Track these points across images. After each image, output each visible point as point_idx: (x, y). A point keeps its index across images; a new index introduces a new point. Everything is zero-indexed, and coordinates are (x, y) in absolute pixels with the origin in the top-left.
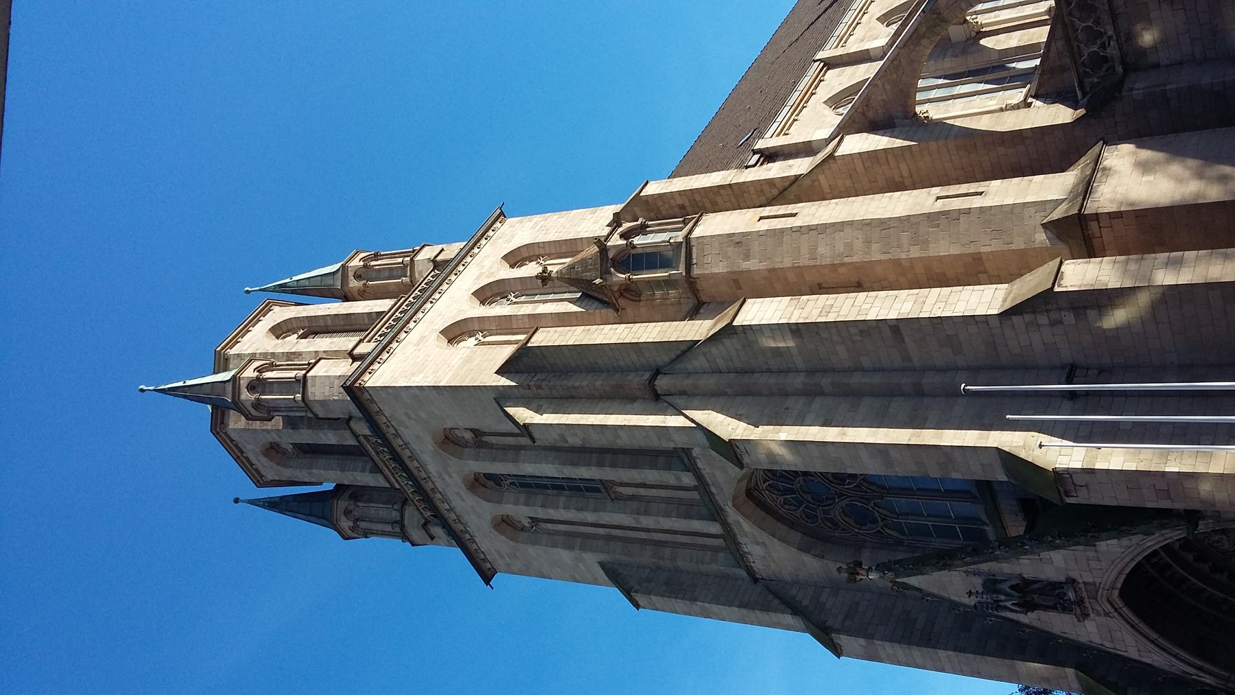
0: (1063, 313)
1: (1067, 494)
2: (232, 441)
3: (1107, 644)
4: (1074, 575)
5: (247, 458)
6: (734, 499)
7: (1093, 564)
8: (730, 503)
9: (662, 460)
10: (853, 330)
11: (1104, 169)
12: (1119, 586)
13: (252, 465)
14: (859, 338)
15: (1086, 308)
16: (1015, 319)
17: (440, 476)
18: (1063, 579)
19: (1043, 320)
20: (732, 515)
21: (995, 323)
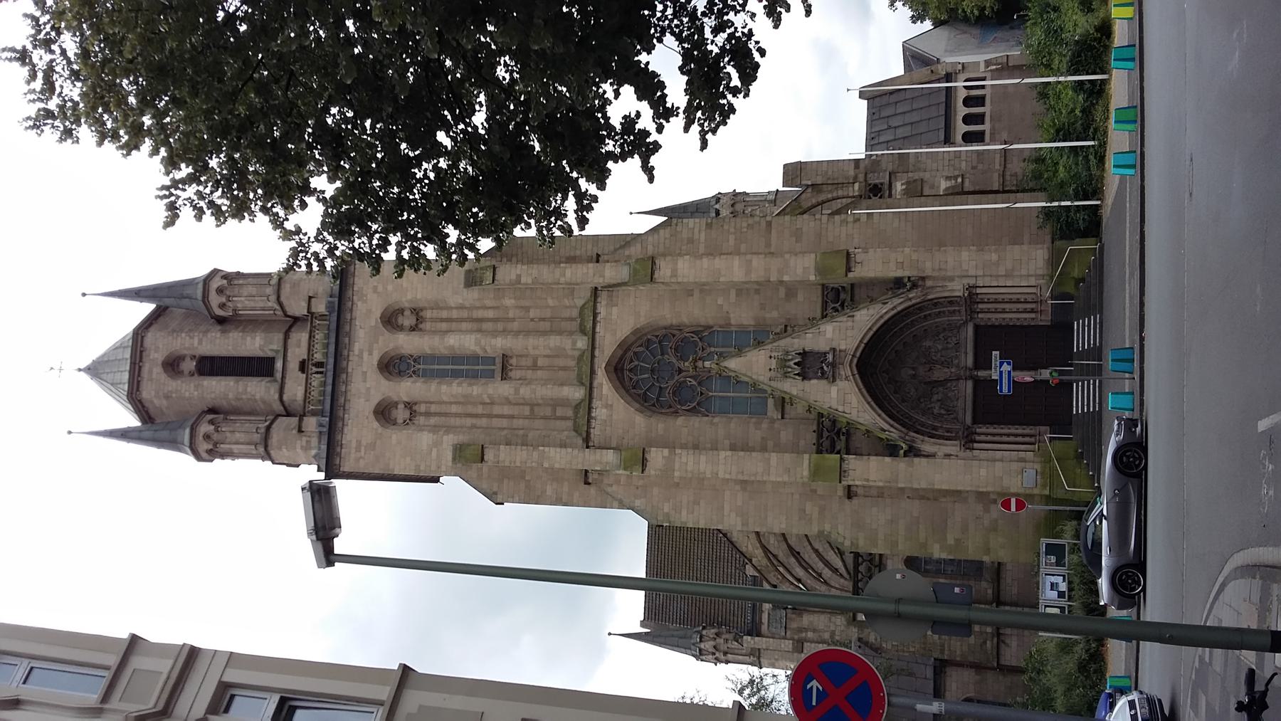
7: (849, 333)
12: (858, 354)
17: (361, 351)
20: (602, 378)
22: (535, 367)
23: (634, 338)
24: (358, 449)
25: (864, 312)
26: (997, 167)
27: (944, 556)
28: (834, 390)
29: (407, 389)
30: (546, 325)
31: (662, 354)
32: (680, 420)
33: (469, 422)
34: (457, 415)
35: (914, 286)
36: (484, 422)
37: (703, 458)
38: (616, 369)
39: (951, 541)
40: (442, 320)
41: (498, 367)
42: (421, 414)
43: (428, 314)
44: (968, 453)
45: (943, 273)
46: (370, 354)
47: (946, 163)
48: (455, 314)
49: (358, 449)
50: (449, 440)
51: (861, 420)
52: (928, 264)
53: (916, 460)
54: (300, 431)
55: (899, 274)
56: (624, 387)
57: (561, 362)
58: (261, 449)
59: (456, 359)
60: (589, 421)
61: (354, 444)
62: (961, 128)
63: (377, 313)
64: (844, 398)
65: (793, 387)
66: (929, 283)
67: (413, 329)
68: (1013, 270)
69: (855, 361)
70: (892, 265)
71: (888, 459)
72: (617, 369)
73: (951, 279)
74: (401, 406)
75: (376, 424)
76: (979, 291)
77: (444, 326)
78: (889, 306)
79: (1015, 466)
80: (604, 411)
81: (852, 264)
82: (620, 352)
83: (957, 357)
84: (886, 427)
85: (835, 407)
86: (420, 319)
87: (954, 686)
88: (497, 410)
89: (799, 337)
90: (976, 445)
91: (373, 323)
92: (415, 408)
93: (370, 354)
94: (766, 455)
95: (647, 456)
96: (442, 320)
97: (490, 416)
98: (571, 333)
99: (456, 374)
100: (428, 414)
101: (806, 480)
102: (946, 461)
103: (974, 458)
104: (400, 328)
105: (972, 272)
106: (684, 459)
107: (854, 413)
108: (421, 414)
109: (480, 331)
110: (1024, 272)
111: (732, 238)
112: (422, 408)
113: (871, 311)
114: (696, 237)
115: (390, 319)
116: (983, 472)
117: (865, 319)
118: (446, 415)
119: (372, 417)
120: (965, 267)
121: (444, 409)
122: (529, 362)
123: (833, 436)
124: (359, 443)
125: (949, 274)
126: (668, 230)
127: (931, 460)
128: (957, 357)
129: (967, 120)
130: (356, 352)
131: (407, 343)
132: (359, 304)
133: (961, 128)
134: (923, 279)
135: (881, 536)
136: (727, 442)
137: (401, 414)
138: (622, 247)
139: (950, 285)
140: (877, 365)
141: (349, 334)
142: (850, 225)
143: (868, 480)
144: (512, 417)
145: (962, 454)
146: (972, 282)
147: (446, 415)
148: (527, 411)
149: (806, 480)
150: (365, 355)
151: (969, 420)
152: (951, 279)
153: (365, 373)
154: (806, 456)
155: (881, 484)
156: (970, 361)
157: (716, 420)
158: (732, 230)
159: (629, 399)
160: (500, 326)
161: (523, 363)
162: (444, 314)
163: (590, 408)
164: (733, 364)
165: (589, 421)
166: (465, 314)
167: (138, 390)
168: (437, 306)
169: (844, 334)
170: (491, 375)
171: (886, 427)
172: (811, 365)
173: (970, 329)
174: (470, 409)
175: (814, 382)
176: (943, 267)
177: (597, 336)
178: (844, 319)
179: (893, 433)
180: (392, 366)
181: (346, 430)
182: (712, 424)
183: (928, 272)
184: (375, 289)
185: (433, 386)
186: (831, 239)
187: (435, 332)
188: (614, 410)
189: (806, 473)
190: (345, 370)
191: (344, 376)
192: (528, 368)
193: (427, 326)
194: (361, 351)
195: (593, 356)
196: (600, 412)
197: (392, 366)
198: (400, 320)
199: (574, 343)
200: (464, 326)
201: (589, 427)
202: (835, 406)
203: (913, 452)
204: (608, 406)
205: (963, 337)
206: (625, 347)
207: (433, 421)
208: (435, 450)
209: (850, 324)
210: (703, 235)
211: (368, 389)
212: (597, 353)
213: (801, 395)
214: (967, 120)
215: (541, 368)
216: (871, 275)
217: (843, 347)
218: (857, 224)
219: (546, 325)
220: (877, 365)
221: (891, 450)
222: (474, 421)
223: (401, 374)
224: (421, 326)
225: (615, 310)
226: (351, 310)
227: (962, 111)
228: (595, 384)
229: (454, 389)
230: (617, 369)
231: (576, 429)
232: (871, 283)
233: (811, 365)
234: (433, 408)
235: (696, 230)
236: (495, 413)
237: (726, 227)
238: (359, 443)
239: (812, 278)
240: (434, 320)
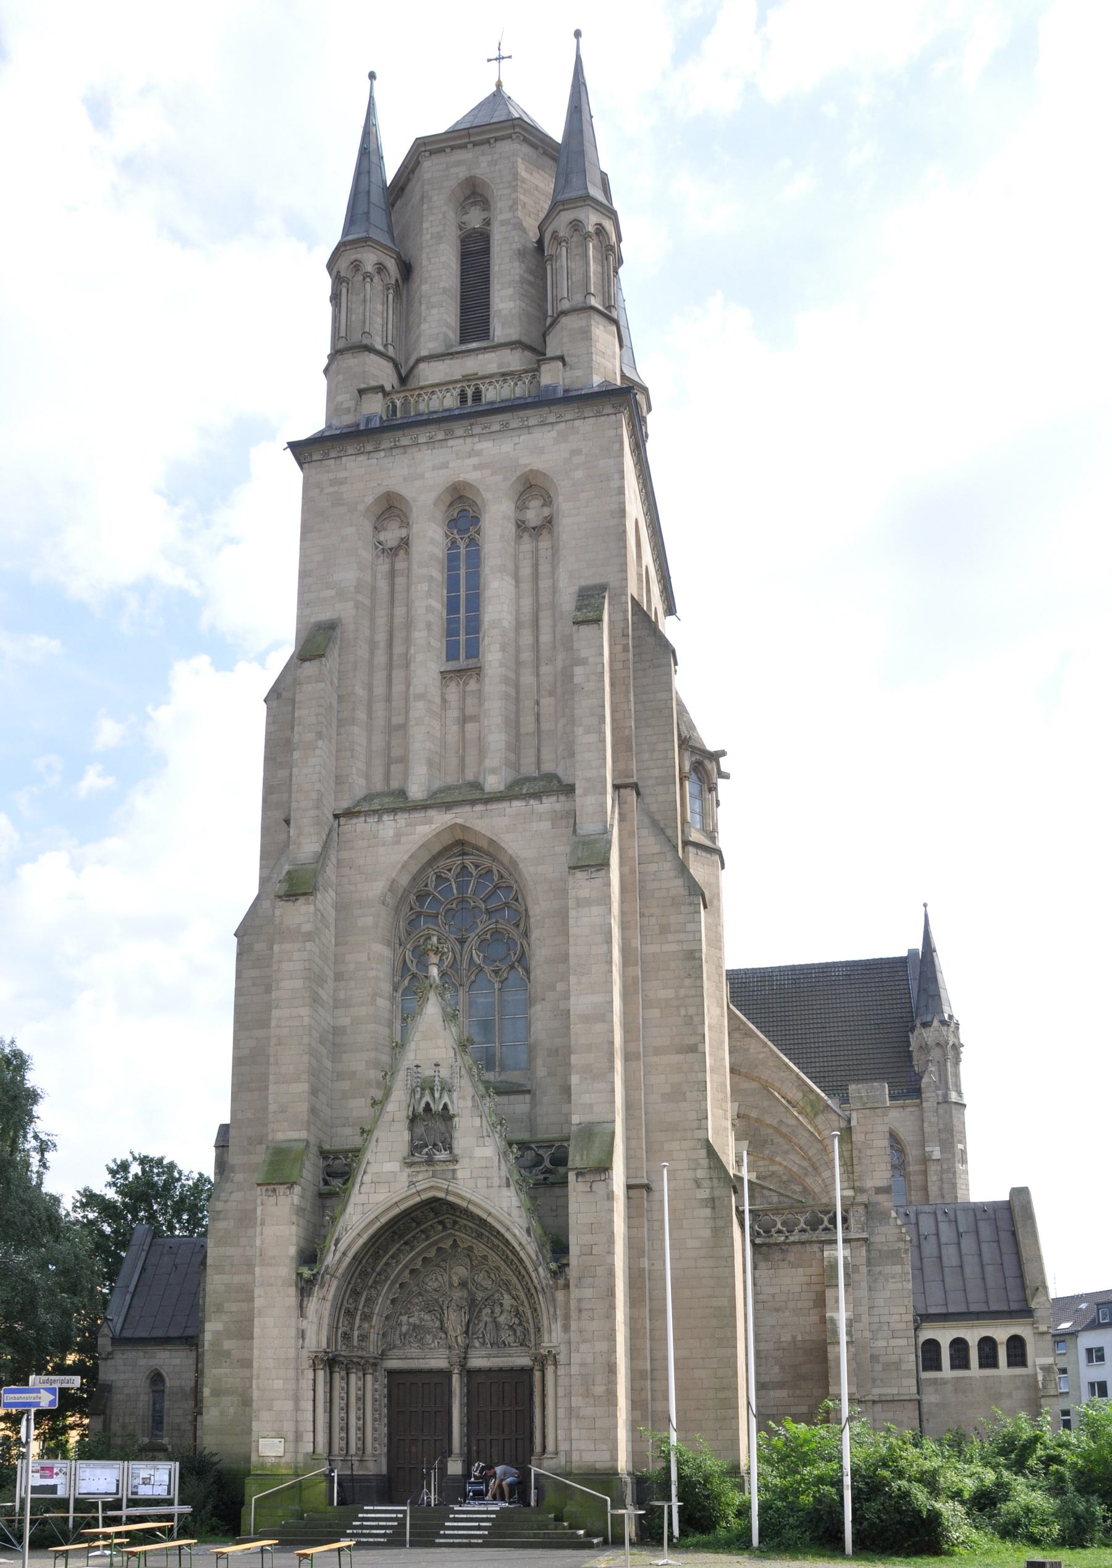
0: (708, 1190)
1: (577, 1175)
2: (497, 139)
3: (367, 1178)
4: (464, 1162)
5: (464, 146)
6: (464, 828)
7: (482, 1182)
8: (460, 821)
9: (512, 757)
10: (692, 1011)
11: (274, 1190)
12: (450, 1198)
13: (453, 148)
14: (683, 1013)
15: (714, 1208)
16: (703, 1153)
17: (479, 453)
18: (456, 1151)
19: (701, 1174)
20: (440, 820)
21: (699, 1134)
22: (464, 720)
23: (506, 861)
24: (335, 482)
25: (515, 1201)
26: (876, 1391)
27: (208, 1336)
28: (393, 1166)
29: (429, 537)
30: (528, 724)
31: (488, 912)
32: (381, 950)
33: (381, 637)
34: (391, 616)
35: (555, 1274)
36: (381, 658)
37: (299, 984)
38: (461, 843)
39: (227, 1344)
40: (536, 566)
41: (462, 663)
42: (392, 564)
43: (544, 544)
44: (306, 1363)
45: (574, 1315)
46: (475, 468)
47: (884, 1319)
48: (545, 584)
49: (335, 482)
50: (345, 611)
51: (350, 1209)
52: (588, 1293)
53: (293, 1291)
54: (361, 392)
55: (574, 1250)
56: (435, 858)
57: (471, 758)
58: (341, 344)
59: (475, 603)
60: (375, 812)
61: (342, 475)
62: (945, 1336)
63: (538, 464)
64: (383, 1185)
65: (397, 1106)
66: (560, 1295)
67: (521, 526)
68: (578, 1417)
69: (441, 1195)
70: (587, 1239)
71: (293, 1251)
72: (459, 845)
73: (566, 1328)
74: (403, 533)
75: (370, 499)
76: (550, 1369)
77: (526, 571)
78: (524, 1238)
79: (288, 1427)
80: (391, 833)
81: (588, 1178)
82: (484, 844)
83: (484, 1344)
84: (342, 1246)
85: (370, 1169)
86: (536, 531)
87: (177, 1361)
88: (398, 675)
89: (475, 1106)
90: (321, 1374)
91: (522, 461)
92: (402, 553)
93: (475, 468)
94: (305, 1076)
95: (302, 900)
96: (536, 566)
97: (390, 666)
98: (516, 766)
99: (452, 606)
100: (392, 574)
101: (270, 1138)
102: (293, 1332)
103: (299, 1373)
104: (521, 505)
105: (576, 1358)
106: (296, 956)
107: (362, 1199)
108: (392, 564)
109: (518, 626)
110: (575, 1433)
111: (670, 993)
112: (400, 565)
113: (515, 1213)
114: (670, 937)
115: (532, 487)
116: (278, 1384)
117: (503, 1204)
118: (392, 601)
119: (381, 490)
120: (583, 1347)
121: (399, 597)
122: (470, 710)
123: (337, 1172)
124: (343, 481)
125: (574, 1325)
126: (683, 892)
127: (295, 1312)
128: (484, 1344)
129: (959, 1346)
130: (478, 447)
131: (497, 517)
132: (554, 434)
133: (945, 1336)
134: (567, 1286)
135: (230, 1251)
136: (346, 1021)
137: (391, 535)
138: (655, 823)
139: (557, 1327)
140: (429, 1225)
141: (505, 428)
142: (690, 1174)
143: (263, 1224)
144: (388, 699)
145: (305, 1354)
146: (562, 1358)
147: (392, 601)
148: (396, 720)
149: (270, 1138)
150: (474, 461)
151: (393, 1364)
152: (566, 1328)
153: (445, 465)
154: (303, 1135)
155: (258, 1243)
156: (477, 1362)
157: (383, 1003)
158: (682, 992)
159: (414, 868)
160: (527, 656)
161: (470, 701)
162: (544, 568)
163: (394, 811)
164: (432, 1009)
165: (375, 812)
166: (545, 599)
167: (525, 140)
168: (555, 551)
169: (482, 1176)
170: (452, 653)
171: (342, 1246)
172: (431, 1132)
173: (524, 1361)
174: (399, 636)
175: (406, 1136)
176: (584, 1314)
177: (506, 804)
178: (504, 1172)
179: (338, 1255)
180: (462, 511)
181: (361, 458)
182: (375, 995)
183: (575, 1293)
184: (576, 452)
185: (438, 574)
186: (666, 1147)
187: (516, 559)
188: (393, 846)
189: (280, 1136)
190: (450, 435)
191: (440, 436)
192: (463, 710)
193: (527, 545)
194: (479, 453)
195: (473, 802)
196: (388, 826)
197: (462, 511)
198: (535, 504)
199: (493, 771)
200: (527, 602)
201: (367, 813)
202: (371, 1169)
203: (305, 1287)
204: (397, 839)
205: (512, 1351)
206: (492, 850)
207: (383, 585)
208: (330, 593)
209: (496, 1182)
210: (673, 947)
211: (421, 476)
212: (479, 808)
213: (386, 1118)
214: (988, 1346)
215: (463, 730)
216: (572, 1208)
217: (460, 1174)
218: (691, 1184)
219: (528, 724)
220: (429, 1225)
221: (309, 1256)
222: (382, 645)
223: (452, 523)
224: (526, 537)
225: (545, 825)
226: (543, 424)
227: (1001, 1333)
228: (432, 813)
229: (427, 602)
230: (459, 845)
231: (368, 798)
232: (561, 1210)
233: (431, 1132)
234: (400, 581)
235: (682, 936)
236: (394, 673)
237: (687, 982)
238: (343, 481)
239: (575, 1119)
240: (536, 553)
